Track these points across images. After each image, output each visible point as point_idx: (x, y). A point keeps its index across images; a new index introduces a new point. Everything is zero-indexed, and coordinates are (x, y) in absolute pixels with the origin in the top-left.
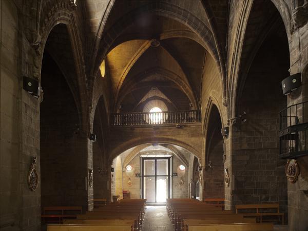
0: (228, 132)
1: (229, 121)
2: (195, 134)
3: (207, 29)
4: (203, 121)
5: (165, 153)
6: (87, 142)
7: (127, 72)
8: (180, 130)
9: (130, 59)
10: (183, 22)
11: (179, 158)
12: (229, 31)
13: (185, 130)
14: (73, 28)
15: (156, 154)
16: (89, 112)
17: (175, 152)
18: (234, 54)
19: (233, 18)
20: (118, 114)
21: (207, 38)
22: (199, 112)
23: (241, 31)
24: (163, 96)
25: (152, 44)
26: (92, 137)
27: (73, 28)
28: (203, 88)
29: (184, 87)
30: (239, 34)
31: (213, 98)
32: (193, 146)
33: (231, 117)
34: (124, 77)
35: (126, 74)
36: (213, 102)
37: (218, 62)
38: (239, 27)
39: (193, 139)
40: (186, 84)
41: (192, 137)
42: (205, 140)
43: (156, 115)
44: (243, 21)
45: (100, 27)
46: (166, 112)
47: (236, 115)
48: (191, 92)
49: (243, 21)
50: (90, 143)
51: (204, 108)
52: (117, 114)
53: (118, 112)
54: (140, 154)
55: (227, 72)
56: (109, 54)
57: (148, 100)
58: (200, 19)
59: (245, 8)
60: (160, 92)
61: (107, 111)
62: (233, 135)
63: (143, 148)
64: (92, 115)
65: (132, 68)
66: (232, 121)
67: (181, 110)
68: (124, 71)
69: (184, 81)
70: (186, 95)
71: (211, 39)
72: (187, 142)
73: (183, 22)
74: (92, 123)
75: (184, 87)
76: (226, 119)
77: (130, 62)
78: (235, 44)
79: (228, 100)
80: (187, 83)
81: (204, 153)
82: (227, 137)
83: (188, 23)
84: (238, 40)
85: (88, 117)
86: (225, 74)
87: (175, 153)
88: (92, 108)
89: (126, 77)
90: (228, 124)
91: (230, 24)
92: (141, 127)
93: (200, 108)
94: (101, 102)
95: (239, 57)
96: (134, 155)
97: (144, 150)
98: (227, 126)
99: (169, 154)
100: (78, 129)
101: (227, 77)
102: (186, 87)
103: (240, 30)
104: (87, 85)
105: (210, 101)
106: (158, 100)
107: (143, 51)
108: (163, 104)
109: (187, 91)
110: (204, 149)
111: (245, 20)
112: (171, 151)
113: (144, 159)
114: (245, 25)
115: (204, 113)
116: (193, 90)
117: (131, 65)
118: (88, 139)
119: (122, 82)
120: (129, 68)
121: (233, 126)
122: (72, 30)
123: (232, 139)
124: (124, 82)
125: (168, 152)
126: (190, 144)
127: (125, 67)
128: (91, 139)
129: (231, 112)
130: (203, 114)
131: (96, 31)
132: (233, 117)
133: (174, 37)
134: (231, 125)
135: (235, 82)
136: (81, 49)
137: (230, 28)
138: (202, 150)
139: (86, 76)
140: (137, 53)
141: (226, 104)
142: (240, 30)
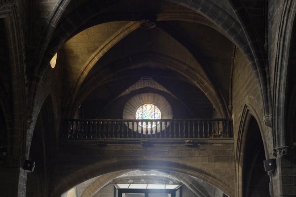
0: (274, 167)
1: (275, 150)
2: (221, 156)
3: (234, 20)
4: (236, 137)
5: (167, 182)
6: (18, 173)
7: (96, 59)
8: (193, 150)
9: (103, 42)
10: (193, 9)
11: (195, 192)
12: (269, 26)
13: (204, 150)
14: (14, 21)
15: (147, 183)
16: (25, 128)
17: (184, 180)
18: (277, 59)
19: (273, 11)
20: (77, 121)
21: (233, 31)
22: (228, 123)
23: (285, 33)
24: (162, 88)
25: (142, 25)
26: (29, 165)
27: (14, 21)
28: (234, 87)
29: (201, 83)
30: (283, 35)
31: (250, 108)
32: (218, 176)
33: (279, 144)
34: (91, 66)
35: (94, 63)
36: (250, 112)
37: (254, 64)
38: (281, 27)
39: (218, 165)
40: (204, 78)
41: (216, 161)
42: (241, 168)
43: (148, 114)
44: (287, 21)
45: (54, 14)
46: (166, 121)
47: (287, 143)
48: (212, 90)
49: (287, 21)
50: (23, 174)
51: (236, 117)
52: (73, 120)
53: (76, 117)
54: (116, 182)
55: (271, 68)
56: (68, 42)
57: (134, 93)
58: (221, 7)
59: (288, 7)
60: (156, 83)
61: (57, 116)
62: (283, 173)
63: (122, 173)
64: (30, 131)
65: (106, 56)
66: (280, 152)
67: (195, 118)
68: (91, 58)
69: (199, 73)
70: (204, 94)
71: (239, 33)
72: (205, 169)
73: (193, 9)
74: (29, 143)
75: (201, 83)
76: (272, 144)
77: (102, 46)
78: (278, 46)
79: (272, 120)
80: (205, 77)
81: (240, 190)
82: (274, 173)
83: (201, 10)
84: (282, 42)
85: (24, 134)
86: (266, 81)
87: (184, 183)
88: (32, 122)
89: (94, 67)
90: (275, 155)
91: (269, 17)
92: (119, 143)
93: (231, 115)
94: (46, 107)
95: (285, 64)
96: (102, 184)
97: (123, 175)
98: (272, 157)
99: (174, 184)
100: (5, 154)
101: (270, 87)
102: (203, 83)
103: (283, 31)
104: (27, 89)
105: (246, 111)
106: (152, 94)
107: (126, 32)
108: (162, 100)
109: (207, 89)
110: (240, 183)
111: (290, 21)
112: (176, 179)
113: (122, 191)
114: (290, 27)
115: (238, 125)
116: (216, 88)
117: (105, 50)
118: (21, 169)
119: (86, 73)
120: (101, 54)
121: (283, 158)
122: (12, 23)
123: (284, 179)
124: (90, 73)
125: (171, 180)
126: (212, 173)
127: (94, 51)
128: (25, 168)
129: (278, 138)
130: (236, 127)
131: (50, 17)
132: (282, 145)
133: (178, 19)
134: (279, 156)
135: (282, 95)
136: (22, 43)
137: (270, 23)
138: (237, 184)
139: (26, 77)
140: (115, 34)
141: (271, 124)
142: (283, 31)
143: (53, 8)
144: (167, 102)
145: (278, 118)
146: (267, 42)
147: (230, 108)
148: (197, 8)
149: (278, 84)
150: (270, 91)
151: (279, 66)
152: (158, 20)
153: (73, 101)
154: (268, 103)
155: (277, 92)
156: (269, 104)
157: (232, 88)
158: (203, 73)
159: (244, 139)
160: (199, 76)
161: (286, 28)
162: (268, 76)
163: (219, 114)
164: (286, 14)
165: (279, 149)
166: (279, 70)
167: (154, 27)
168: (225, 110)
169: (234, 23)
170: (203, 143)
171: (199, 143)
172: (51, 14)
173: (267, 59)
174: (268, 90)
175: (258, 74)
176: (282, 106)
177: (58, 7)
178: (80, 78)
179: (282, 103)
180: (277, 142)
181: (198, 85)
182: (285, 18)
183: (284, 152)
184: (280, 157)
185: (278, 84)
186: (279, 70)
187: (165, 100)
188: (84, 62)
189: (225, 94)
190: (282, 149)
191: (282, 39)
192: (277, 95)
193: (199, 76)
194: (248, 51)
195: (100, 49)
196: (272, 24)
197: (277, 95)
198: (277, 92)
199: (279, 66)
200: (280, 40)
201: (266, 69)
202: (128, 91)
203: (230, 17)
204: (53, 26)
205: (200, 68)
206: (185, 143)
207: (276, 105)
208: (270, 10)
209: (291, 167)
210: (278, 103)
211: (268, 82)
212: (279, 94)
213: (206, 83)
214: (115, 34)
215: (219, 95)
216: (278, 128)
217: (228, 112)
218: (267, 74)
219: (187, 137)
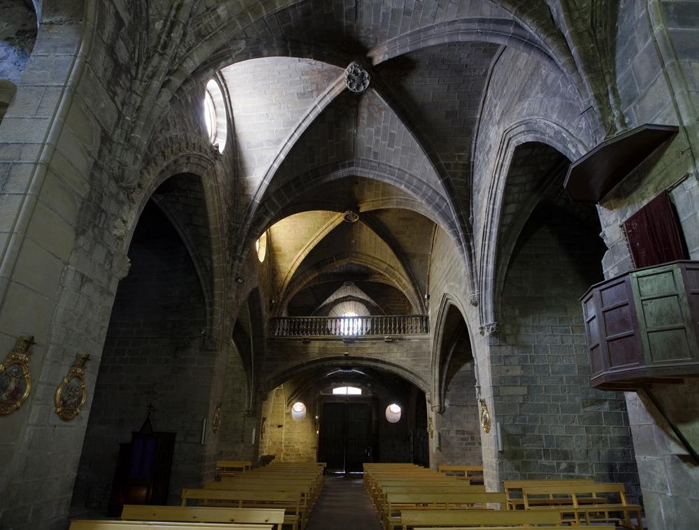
8: (392, 345)
13: (402, 346)
18: (485, 227)
22: (424, 319)
30: (492, 197)
33: (486, 321)
59: (501, 161)
69: (398, 272)
71: (443, 208)
75: (399, 280)
76: (477, 324)
84: (491, 206)
93: (428, 311)
95: (495, 230)
103: (494, 192)
105: (445, 298)
106: (354, 302)
109: (405, 287)
116: (414, 285)
119: (293, 271)
129: (486, 313)
131: (252, 193)
132: (490, 321)
142: (494, 192)
143: (258, 183)
144: (367, 310)
145: (485, 292)
146: (473, 215)
147: (427, 305)
148: (401, 184)
149: (486, 255)
150: (476, 267)
151: (488, 234)
152: (362, 210)
153: (281, 300)
154: (473, 278)
155: (485, 264)
156: (475, 280)
157: (428, 283)
158: (404, 273)
159: (441, 332)
160: (397, 274)
161: (496, 189)
162: (473, 251)
163: (416, 310)
164: (498, 171)
165: (487, 326)
166: (487, 239)
167: (356, 220)
168: (421, 306)
169: (438, 198)
170: (401, 339)
171: (398, 339)
172: (256, 190)
173: (472, 232)
174: (474, 266)
175: (463, 250)
176: (490, 278)
177: (263, 181)
178: (287, 276)
179: (490, 275)
180: (484, 319)
181: (396, 283)
182: (497, 176)
183: (492, 329)
184: (488, 335)
185: (486, 255)
186: (487, 239)
187: (365, 308)
188: (291, 260)
189: (421, 286)
190: (490, 325)
191: (492, 201)
192: (485, 267)
193: (397, 274)
194: (452, 226)
195: (306, 246)
196: (479, 192)
197: (485, 267)
198: (485, 264)
199: (488, 234)
200: (490, 204)
201: (471, 243)
202: (332, 299)
203: (435, 191)
204: (257, 201)
205: (399, 265)
206: (383, 339)
207: (484, 278)
208: (476, 180)
209: (500, 345)
210: (486, 276)
211: (473, 256)
212: (487, 266)
213: (404, 281)
214: (321, 230)
215: (416, 291)
216: (485, 304)
217: (424, 308)
218: (472, 248)
219: (386, 333)
